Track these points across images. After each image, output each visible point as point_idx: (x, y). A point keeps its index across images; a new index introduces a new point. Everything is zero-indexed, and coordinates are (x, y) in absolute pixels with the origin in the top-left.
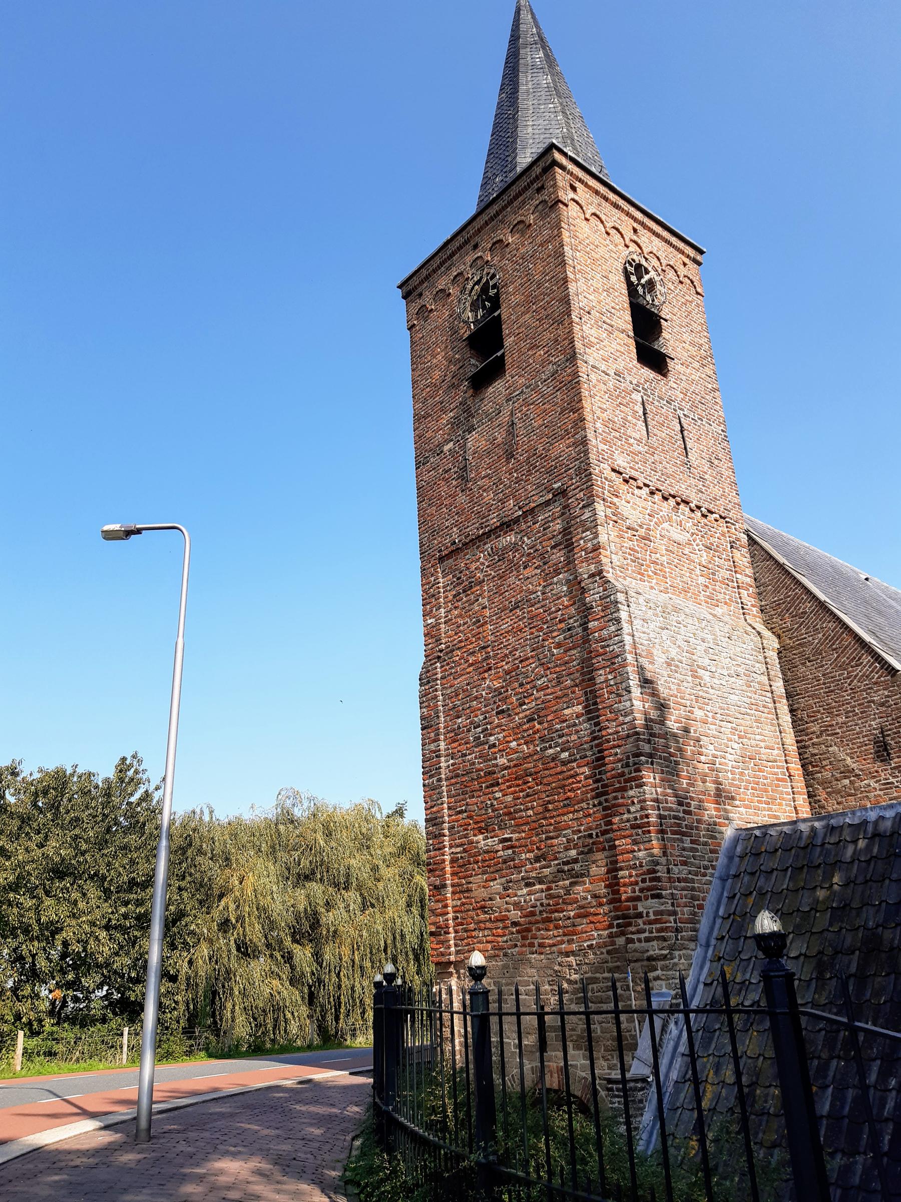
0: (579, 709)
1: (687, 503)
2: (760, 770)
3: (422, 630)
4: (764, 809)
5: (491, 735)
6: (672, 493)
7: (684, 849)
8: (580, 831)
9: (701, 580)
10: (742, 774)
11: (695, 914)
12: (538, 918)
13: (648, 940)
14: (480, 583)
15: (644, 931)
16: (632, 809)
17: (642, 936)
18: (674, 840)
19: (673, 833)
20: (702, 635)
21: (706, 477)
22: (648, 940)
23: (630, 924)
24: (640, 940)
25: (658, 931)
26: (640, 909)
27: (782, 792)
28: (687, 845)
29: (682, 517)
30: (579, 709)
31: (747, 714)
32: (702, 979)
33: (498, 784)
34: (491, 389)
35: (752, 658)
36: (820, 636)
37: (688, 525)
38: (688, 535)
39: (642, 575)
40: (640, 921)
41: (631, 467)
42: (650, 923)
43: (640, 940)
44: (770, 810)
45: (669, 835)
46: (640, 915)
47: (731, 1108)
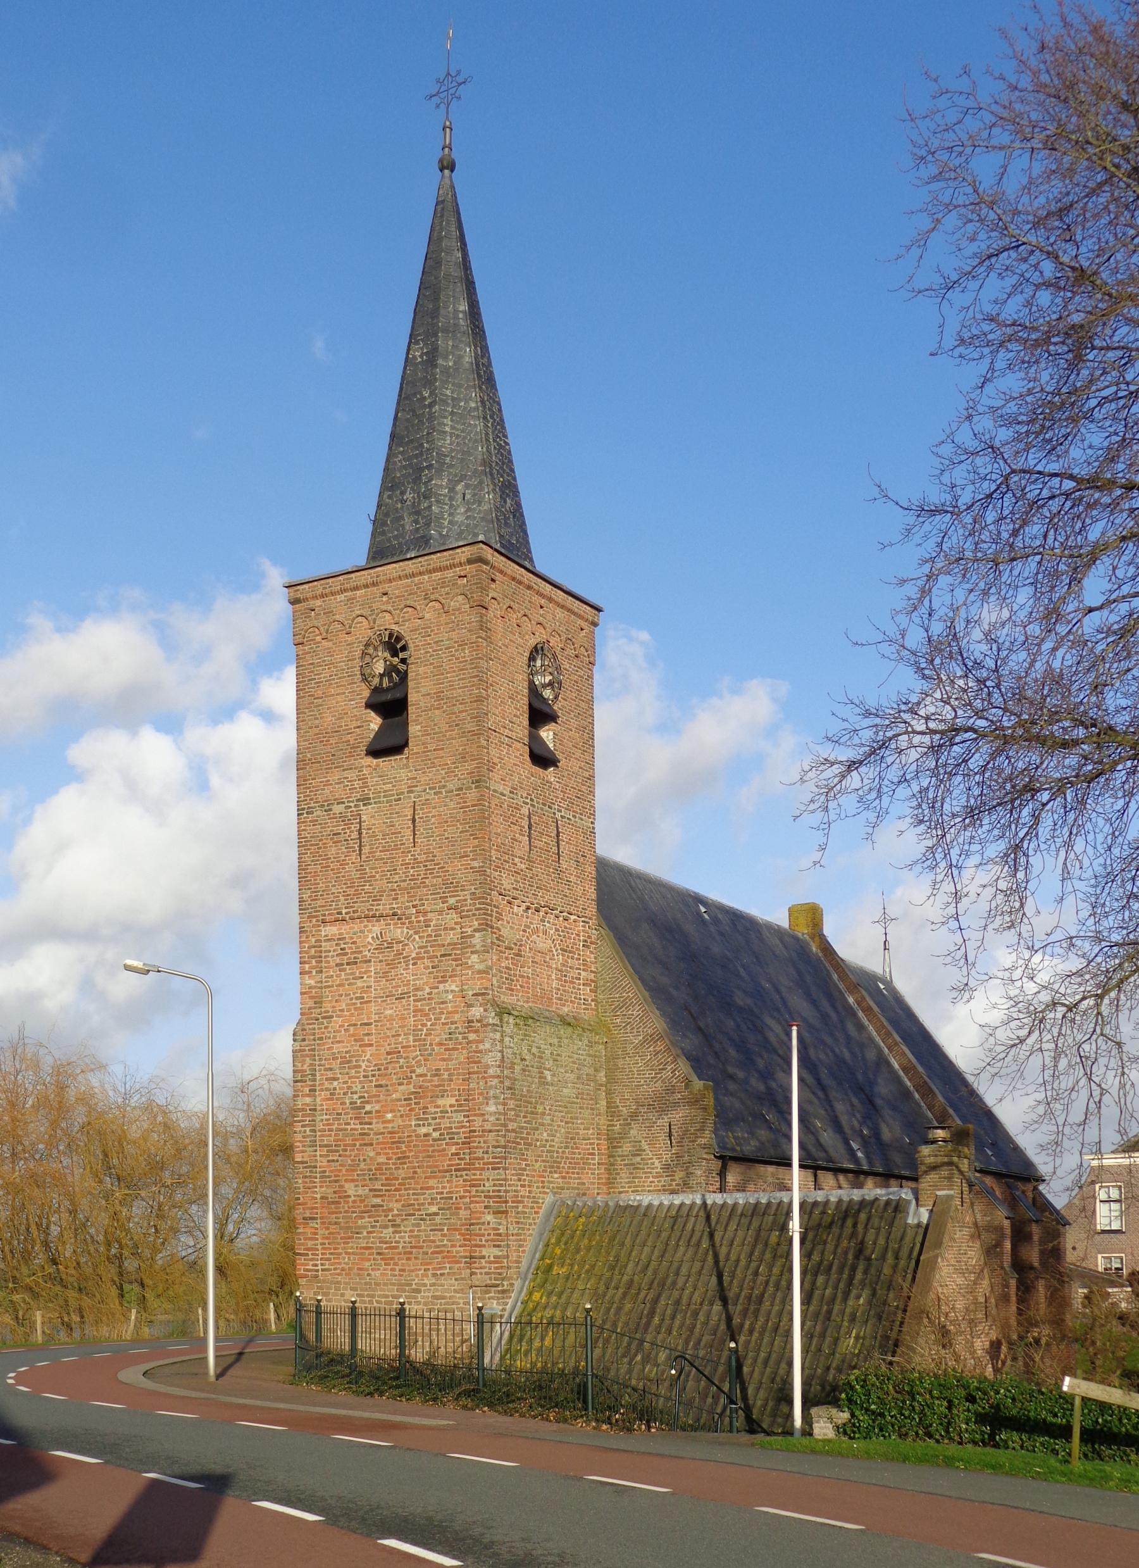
0: (453, 1101)
3: (297, 989)
4: (575, 1178)
5: (368, 1102)
7: (518, 1213)
10: (563, 1152)
11: (520, 1257)
14: (366, 962)
15: (485, 1268)
16: (487, 1185)
17: (483, 1271)
18: (513, 1207)
19: (513, 1202)
20: (550, 1040)
24: (481, 1274)
25: (496, 1268)
26: (484, 1253)
27: (590, 1164)
28: (520, 1209)
29: (548, 925)
30: (453, 1101)
31: (574, 1103)
32: (521, 1299)
33: (372, 1144)
34: (373, 714)
35: (584, 1053)
36: (641, 1038)
37: (552, 932)
39: (512, 990)
40: (483, 1261)
41: (514, 888)
42: (491, 1262)
45: (510, 1204)
46: (484, 1257)
47: (1071, 938)
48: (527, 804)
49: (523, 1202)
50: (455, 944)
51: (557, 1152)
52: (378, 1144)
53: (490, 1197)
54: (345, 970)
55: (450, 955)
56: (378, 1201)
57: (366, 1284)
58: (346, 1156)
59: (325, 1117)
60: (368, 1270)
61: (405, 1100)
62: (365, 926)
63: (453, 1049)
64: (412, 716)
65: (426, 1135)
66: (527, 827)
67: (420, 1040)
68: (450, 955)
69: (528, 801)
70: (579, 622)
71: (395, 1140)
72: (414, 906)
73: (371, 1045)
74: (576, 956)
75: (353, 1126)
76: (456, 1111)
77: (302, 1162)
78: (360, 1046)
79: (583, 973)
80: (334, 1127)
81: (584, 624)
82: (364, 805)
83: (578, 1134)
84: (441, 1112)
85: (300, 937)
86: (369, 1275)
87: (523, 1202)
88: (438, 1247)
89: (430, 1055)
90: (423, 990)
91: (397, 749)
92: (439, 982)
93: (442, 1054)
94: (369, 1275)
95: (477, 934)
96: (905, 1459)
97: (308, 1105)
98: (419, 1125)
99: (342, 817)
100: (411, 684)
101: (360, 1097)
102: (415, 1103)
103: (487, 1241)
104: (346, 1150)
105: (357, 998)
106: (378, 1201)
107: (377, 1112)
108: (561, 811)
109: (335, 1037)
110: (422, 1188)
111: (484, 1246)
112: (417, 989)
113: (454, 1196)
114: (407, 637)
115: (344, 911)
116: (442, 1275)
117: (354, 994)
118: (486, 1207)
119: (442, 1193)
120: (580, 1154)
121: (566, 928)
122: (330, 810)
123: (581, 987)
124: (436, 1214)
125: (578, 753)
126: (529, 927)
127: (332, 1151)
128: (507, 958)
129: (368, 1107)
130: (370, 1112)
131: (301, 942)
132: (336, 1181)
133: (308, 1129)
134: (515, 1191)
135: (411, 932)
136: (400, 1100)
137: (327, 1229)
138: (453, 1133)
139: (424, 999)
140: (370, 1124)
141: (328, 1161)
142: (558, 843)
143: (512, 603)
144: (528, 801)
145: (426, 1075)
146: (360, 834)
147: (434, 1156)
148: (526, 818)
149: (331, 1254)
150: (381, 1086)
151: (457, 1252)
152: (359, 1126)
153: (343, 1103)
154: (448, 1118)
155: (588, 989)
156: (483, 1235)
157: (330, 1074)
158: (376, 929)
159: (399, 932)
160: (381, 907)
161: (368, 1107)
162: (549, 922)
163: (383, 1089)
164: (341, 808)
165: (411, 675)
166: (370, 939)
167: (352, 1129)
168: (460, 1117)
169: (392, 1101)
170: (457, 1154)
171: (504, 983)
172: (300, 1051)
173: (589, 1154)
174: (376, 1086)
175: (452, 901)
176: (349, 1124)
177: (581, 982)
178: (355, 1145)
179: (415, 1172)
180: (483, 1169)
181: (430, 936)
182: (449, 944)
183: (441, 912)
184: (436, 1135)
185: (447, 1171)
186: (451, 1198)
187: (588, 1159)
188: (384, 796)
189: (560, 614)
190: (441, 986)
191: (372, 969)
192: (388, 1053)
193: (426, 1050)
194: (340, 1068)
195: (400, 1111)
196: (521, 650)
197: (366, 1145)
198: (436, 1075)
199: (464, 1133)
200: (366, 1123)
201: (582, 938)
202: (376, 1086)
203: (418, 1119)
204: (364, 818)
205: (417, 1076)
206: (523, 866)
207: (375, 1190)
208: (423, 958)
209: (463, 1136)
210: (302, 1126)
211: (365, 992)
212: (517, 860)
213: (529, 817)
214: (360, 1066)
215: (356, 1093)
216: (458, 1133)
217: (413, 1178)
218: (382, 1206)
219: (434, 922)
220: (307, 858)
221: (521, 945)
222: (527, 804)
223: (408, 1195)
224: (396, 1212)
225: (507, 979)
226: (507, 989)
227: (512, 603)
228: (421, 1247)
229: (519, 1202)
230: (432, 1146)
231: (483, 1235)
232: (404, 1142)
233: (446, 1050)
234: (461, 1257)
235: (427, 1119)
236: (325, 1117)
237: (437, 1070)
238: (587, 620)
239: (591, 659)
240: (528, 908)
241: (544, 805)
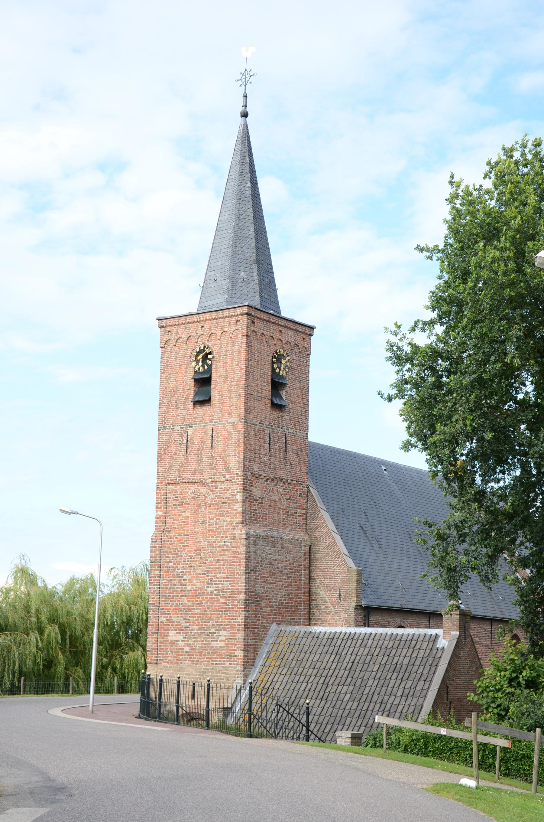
1: (281, 479)
2: (291, 600)
4: (289, 616)
5: (185, 575)
6: (276, 477)
8: (217, 622)
9: (282, 516)
12: (197, 651)
13: (237, 664)
15: (236, 661)
21: (294, 463)
22: (237, 664)
23: (231, 658)
30: (224, 575)
33: (186, 596)
37: (281, 490)
38: (280, 495)
42: (239, 659)
43: (234, 664)
44: (292, 616)
46: (236, 656)
48: (269, 428)
49: (258, 628)
50: (229, 498)
51: (279, 603)
52: (189, 596)
53: (240, 625)
54: (177, 508)
55: (226, 503)
56: (187, 625)
57: (180, 667)
58: (173, 601)
59: (164, 581)
60: (181, 660)
61: (202, 574)
62: (188, 487)
63: (226, 550)
64: (213, 386)
65: (211, 592)
66: (268, 439)
67: (210, 545)
68: (226, 503)
69: (270, 426)
70: (302, 335)
71: (196, 594)
72: (211, 478)
73: (187, 546)
74: (295, 502)
75: (177, 586)
76: (226, 581)
77: (152, 604)
78: (183, 546)
79: (299, 510)
80: (168, 587)
81: (305, 336)
82: (190, 427)
83: (292, 593)
84: (219, 581)
85: (157, 490)
86: (181, 663)
87: (258, 628)
88: (215, 650)
89: (215, 552)
90: (213, 519)
91: (207, 401)
92: (220, 516)
93: (220, 552)
94: (181, 663)
95: (238, 494)
96: (313, 746)
97: (156, 575)
98: (208, 587)
99: (179, 433)
100: (213, 371)
101: (182, 572)
102: (207, 576)
103: (237, 648)
104: (173, 598)
105: (182, 522)
106: (187, 625)
107: (189, 580)
108: (288, 430)
109: (171, 541)
110: (208, 619)
111: (236, 650)
112: (210, 519)
113: (223, 624)
114: (213, 348)
115: (178, 479)
116: (216, 664)
117: (181, 520)
118: (238, 630)
119: (217, 622)
120: (292, 603)
121: (289, 487)
122: (174, 429)
123: (298, 517)
124: (215, 633)
125: (300, 400)
126: (268, 489)
127: (167, 599)
128: (254, 505)
129: (185, 577)
130: (185, 580)
131: (157, 493)
132: (168, 614)
133: (155, 587)
134: (254, 622)
135: (209, 491)
136: (200, 574)
137: (163, 638)
138: (224, 592)
139: (213, 524)
140: (186, 585)
141: (165, 604)
142: (286, 445)
143: (264, 332)
144: (270, 426)
145: (213, 562)
146: (187, 441)
147: (214, 603)
148: (268, 435)
149: (164, 651)
150: (191, 566)
151: (224, 653)
152: (180, 586)
153: (173, 575)
154: (222, 584)
155: (301, 518)
156: (236, 645)
157: (168, 560)
158: (193, 489)
159: (202, 490)
160: (195, 478)
161: (185, 577)
162: (279, 485)
163: (192, 568)
164: (179, 428)
165: (213, 366)
166: (189, 493)
167: (177, 588)
168: (227, 584)
169: (196, 574)
170: (225, 603)
171: (252, 517)
172: (154, 547)
173: (298, 603)
174: (189, 567)
175: (228, 476)
176: (175, 585)
177: (298, 514)
178: (178, 596)
179: (205, 611)
180: (237, 611)
181: (217, 493)
182: (226, 498)
183: (223, 482)
184: (216, 592)
185: (220, 611)
186: (222, 625)
187: (297, 606)
188: (199, 424)
189: (291, 333)
190: (221, 518)
191: (190, 508)
192: (196, 550)
193: (213, 549)
194: (173, 557)
195: (199, 580)
196: (268, 353)
197: (183, 596)
198: (217, 562)
199: (229, 592)
200: (183, 585)
201: (298, 492)
202: (189, 567)
203: (208, 584)
204: (189, 433)
205: (208, 563)
206: (265, 459)
207: (186, 619)
208: (213, 504)
209: (228, 594)
210: (154, 585)
211: (187, 519)
212: (262, 456)
213: (270, 434)
214: (182, 556)
215: (179, 569)
216: (227, 592)
217: (204, 614)
218: (189, 627)
219: (219, 487)
220: (162, 452)
221: (263, 498)
222: (269, 428)
223: (202, 622)
224: (196, 631)
225: (254, 515)
226: (253, 520)
227: (264, 332)
228: (207, 650)
229: (255, 628)
230: (214, 598)
231: (236, 645)
232: (201, 596)
233: (223, 550)
234: (225, 655)
235: (212, 584)
236: (164, 581)
237: (218, 560)
238: (306, 334)
239: (308, 353)
240: (267, 479)
241: (279, 427)
